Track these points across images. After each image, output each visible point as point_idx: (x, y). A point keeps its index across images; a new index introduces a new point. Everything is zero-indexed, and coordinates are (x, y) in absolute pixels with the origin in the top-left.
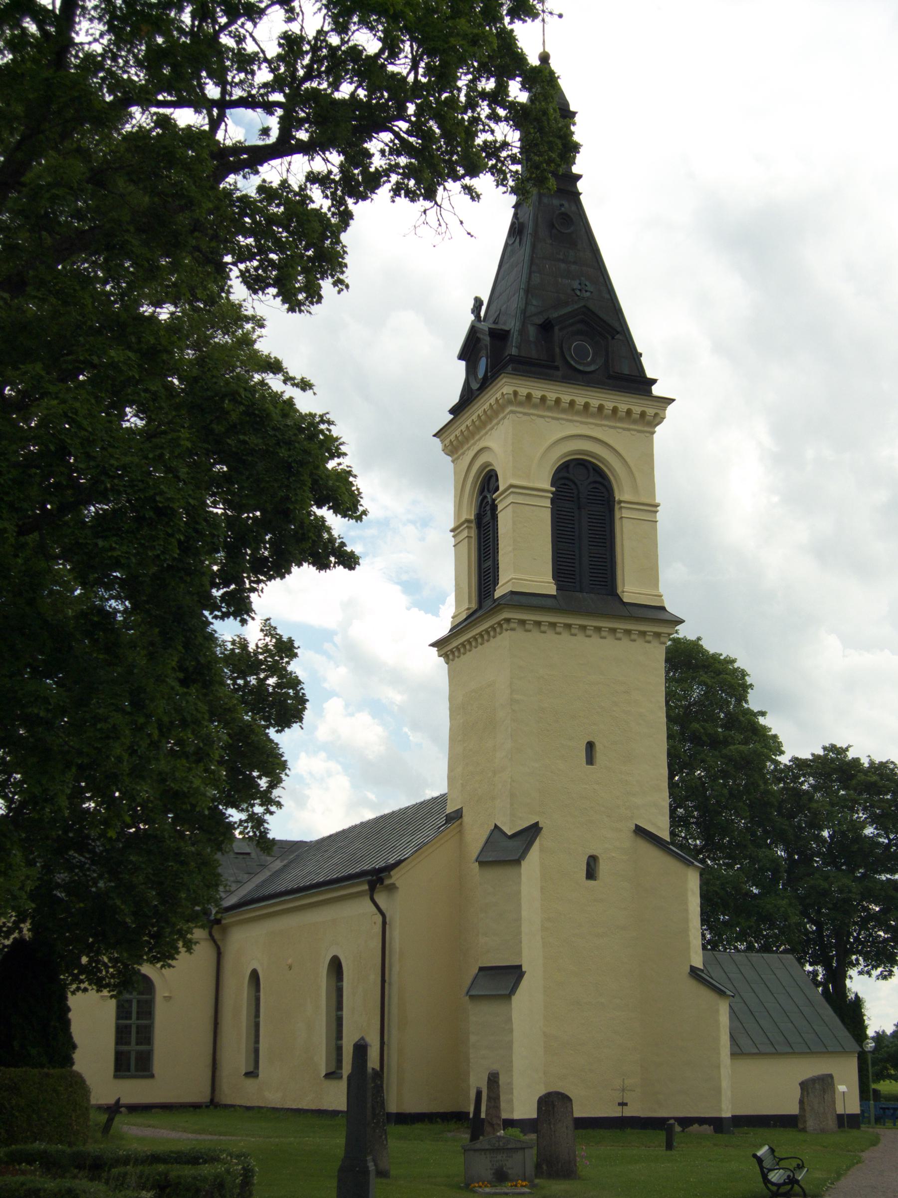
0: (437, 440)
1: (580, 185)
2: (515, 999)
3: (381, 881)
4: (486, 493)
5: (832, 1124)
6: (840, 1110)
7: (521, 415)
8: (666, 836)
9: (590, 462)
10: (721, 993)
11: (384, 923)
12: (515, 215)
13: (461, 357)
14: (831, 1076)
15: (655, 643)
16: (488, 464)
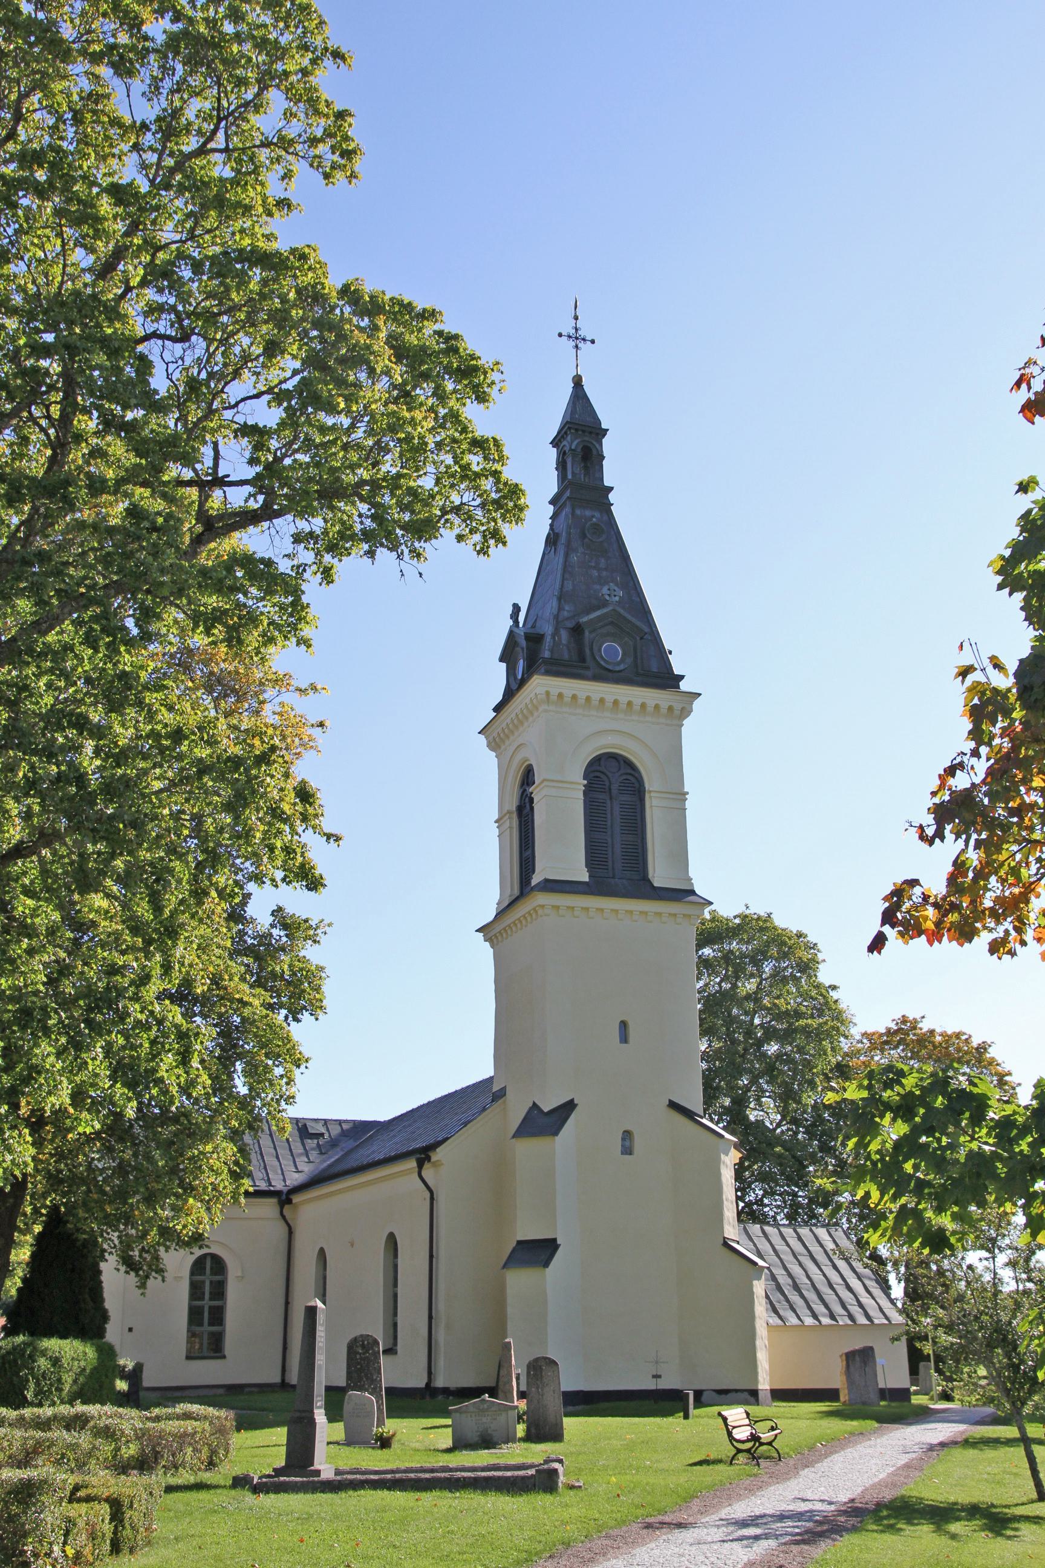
0: (482, 737)
1: (611, 497)
5: (874, 1396)
6: (881, 1385)
9: (621, 756)
11: (432, 1198)
12: (551, 525)
13: (501, 660)
14: (871, 1349)
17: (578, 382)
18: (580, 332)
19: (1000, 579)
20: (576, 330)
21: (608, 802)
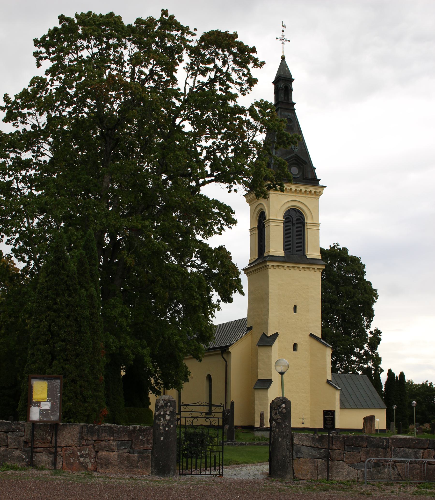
1: (295, 111)
2: (269, 390)
3: (225, 350)
4: (261, 219)
6: (376, 428)
7: (273, 194)
8: (320, 336)
10: (337, 389)
14: (374, 416)
15: (318, 271)
16: (262, 209)
17: (283, 58)
18: (284, 37)
19: (397, 374)
20: (283, 43)
21: (292, 226)
